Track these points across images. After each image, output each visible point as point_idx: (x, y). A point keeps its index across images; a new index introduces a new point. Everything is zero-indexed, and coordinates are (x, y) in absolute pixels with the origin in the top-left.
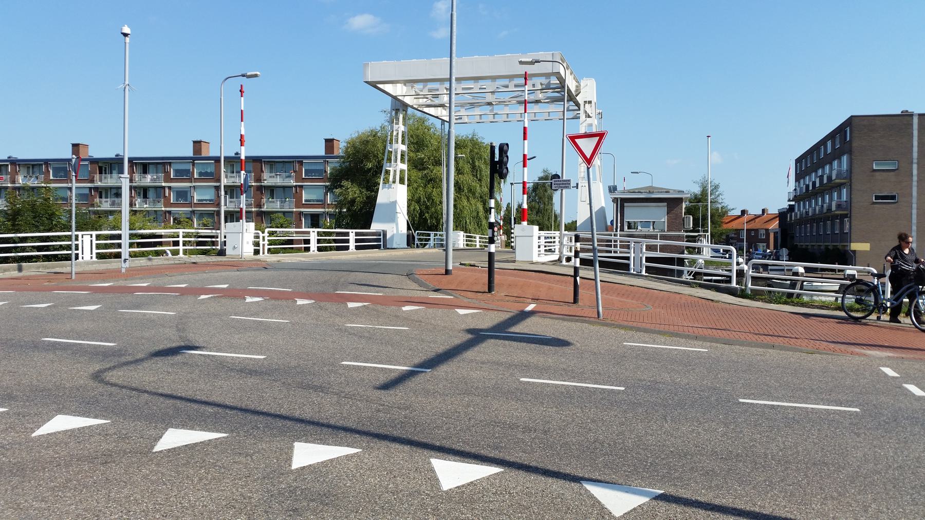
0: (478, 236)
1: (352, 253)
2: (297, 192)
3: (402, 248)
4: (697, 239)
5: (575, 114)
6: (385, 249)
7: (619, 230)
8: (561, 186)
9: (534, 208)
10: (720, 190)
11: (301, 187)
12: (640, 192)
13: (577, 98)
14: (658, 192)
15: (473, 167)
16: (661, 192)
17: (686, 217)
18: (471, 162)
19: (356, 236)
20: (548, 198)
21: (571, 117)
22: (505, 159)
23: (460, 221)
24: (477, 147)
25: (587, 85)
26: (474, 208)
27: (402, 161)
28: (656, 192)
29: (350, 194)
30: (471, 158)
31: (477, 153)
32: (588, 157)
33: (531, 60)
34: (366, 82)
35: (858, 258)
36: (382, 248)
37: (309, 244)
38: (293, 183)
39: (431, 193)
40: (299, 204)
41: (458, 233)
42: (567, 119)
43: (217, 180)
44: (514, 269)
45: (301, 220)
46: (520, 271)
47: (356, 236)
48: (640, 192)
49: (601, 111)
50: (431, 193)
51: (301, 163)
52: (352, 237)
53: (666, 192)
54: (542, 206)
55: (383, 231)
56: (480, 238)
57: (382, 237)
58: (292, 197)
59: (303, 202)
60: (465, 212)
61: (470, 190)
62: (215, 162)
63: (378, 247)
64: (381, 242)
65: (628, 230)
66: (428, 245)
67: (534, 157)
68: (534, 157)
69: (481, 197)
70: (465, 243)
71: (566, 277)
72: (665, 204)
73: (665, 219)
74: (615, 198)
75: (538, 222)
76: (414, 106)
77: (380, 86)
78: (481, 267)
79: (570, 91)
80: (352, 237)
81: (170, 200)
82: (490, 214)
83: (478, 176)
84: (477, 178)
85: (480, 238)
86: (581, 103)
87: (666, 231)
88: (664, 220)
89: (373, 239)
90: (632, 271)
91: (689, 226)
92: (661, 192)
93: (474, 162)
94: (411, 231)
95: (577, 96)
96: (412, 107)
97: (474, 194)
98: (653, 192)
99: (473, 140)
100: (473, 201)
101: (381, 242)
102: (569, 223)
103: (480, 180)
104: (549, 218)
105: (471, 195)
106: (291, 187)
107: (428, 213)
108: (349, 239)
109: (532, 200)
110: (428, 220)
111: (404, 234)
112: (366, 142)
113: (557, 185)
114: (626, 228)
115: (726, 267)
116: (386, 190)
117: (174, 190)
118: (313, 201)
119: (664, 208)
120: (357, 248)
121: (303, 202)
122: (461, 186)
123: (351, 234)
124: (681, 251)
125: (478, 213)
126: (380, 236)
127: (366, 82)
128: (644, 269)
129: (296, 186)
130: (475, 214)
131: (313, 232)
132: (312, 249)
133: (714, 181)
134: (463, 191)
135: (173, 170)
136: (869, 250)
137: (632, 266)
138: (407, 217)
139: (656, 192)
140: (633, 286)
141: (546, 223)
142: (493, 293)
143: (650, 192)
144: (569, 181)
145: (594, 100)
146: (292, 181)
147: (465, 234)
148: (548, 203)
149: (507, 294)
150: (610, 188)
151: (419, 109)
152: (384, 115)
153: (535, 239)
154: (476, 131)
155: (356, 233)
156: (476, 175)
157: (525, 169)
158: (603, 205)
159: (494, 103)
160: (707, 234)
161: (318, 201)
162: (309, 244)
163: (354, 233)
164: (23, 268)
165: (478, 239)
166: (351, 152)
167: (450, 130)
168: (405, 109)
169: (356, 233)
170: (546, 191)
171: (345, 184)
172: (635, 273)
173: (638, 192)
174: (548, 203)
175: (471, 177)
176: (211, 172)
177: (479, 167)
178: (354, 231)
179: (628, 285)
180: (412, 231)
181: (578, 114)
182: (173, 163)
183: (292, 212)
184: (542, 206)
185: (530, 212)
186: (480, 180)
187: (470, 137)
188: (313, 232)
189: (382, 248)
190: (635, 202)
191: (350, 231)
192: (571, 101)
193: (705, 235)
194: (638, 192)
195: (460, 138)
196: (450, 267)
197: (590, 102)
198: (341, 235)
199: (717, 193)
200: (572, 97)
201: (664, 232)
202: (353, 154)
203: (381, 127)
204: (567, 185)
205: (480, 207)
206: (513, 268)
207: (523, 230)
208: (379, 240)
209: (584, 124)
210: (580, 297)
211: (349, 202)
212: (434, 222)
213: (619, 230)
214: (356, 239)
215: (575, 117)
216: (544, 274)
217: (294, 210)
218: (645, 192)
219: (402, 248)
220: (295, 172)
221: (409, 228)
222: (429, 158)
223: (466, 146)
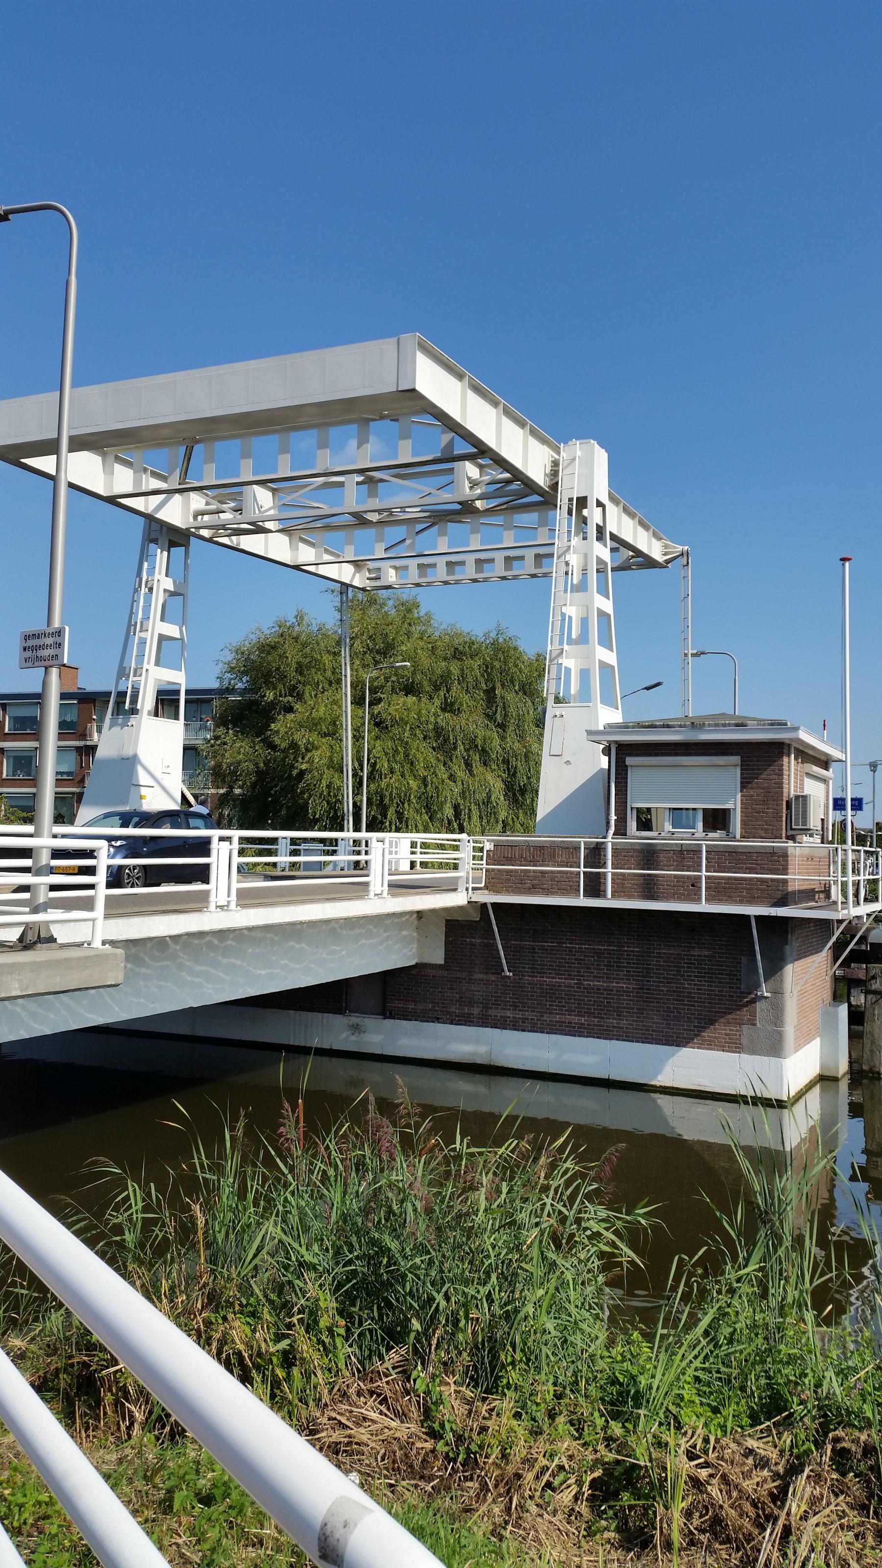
16: (724, 725)
24: (500, 655)
28: (709, 725)
35: (832, 1009)
43: (81, 735)
48: (668, 726)
53: (737, 725)
62: (79, 703)
65: (638, 834)
66: (331, 867)
72: (736, 759)
77: (123, 501)
81: (2, 773)
87: (738, 836)
92: (724, 725)
103: (502, 726)
108: (207, 867)
112: (268, 648)
114: (632, 825)
116: (117, 729)
117: (10, 754)
119: (732, 769)
123: (215, 845)
124: (779, 895)
131: (222, 839)
135: (10, 718)
136: (443, 962)
139: (709, 725)
152: (330, 596)
176: (72, 721)
177: (502, 698)
182: (10, 704)
186: (502, 726)
188: (222, 839)
190: (656, 755)
198: (162, 845)
201: (734, 839)
203: (296, 617)
218: (681, 726)
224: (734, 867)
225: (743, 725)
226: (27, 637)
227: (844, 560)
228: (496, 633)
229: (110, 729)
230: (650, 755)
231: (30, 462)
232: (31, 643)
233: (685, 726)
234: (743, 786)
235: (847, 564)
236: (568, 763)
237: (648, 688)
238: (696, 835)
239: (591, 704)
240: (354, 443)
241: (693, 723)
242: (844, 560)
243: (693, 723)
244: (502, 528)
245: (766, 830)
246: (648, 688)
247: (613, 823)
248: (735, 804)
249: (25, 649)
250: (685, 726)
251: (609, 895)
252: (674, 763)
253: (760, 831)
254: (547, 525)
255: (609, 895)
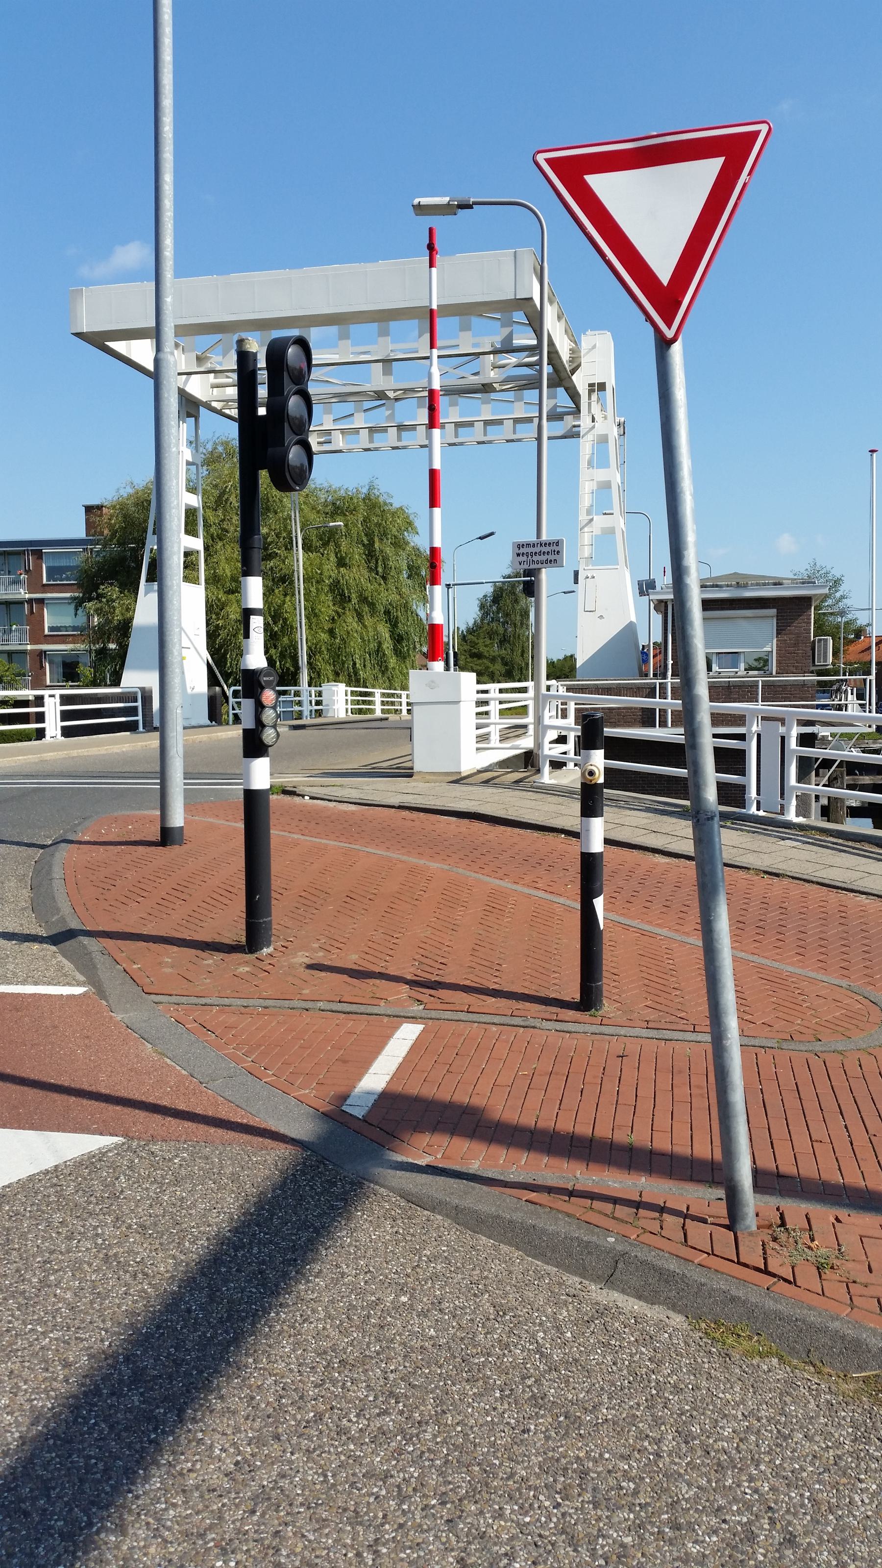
0: (378, 692)
1: (53, 747)
2: (32, 612)
3: (194, 727)
4: (835, 687)
5: (569, 427)
6: (148, 731)
7: (670, 673)
8: (535, 558)
9: (497, 633)
10: (843, 589)
11: (41, 601)
12: (717, 586)
13: (574, 378)
14: (758, 584)
15: (370, 554)
16: (764, 584)
17: (820, 640)
18: (366, 542)
19: (62, 704)
20: (521, 615)
21: (560, 433)
22: (294, 403)
23: (343, 663)
25: (594, 347)
26: (371, 634)
27: (191, 530)
28: (752, 585)
29: (117, 611)
30: (366, 535)
31: (378, 525)
32: (665, 277)
33: (445, 200)
34: (78, 335)
36: (141, 728)
37: (44, 722)
38: (23, 594)
39: (281, 606)
40: (37, 636)
41: (334, 688)
42: (549, 438)
44: (401, 807)
45: (42, 667)
46: (415, 815)
47: (62, 704)
48: (717, 586)
49: (622, 420)
50: (281, 606)
51: (39, 555)
52: (52, 708)
53: (775, 584)
54: (510, 630)
55: (143, 689)
56: (383, 695)
57: (139, 704)
58: (25, 622)
59: (46, 632)
60: (352, 644)
61: (363, 599)
63: (131, 727)
64: (137, 715)
67: (492, 534)
68: (492, 534)
69: (387, 612)
70: (350, 707)
71: (551, 836)
72: (773, 612)
73: (771, 647)
74: (660, 601)
75: (502, 659)
76: (214, 404)
77: (118, 346)
78: (312, 798)
79: (557, 352)
80: (52, 708)
82: (247, 635)
83: (380, 570)
84: (377, 574)
85: (383, 695)
86: (582, 388)
87: (774, 673)
88: (770, 649)
89: (119, 708)
90: (753, 810)
91: (825, 660)
92: (764, 584)
93: (372, 543)
94: (217, 688)
95: (573, 371)
96: (208, 406)
97: (372, 605)
98: (745, 586)
99: (370, 499)
100: (369, 621)
101: (137, 715)
102: (559, 660)
104: (523, 652)
105: (366, 609)
106: (20, 603)
107: (275, 647)
108: (63, 720)
109: (493, 618)
110: (276, 662)
111: (199, 695)
113: (525, 558)
115: (874, 743)
118: (66, 628)
120: (67, 732)
121: (46, 632)
122: (343, 591)
123: (47, 700)
125: (380, 644)
126: (136, 701)
127: (78, 335)
128: (794, 802)
129: (30, 601)
130: (373, 645)
131: (51, 696)
132: (48, 733)
133: (833, 572)
134: (350, 601)
137: (753, 793)
138: (206, 655)
139: (752, 585)
140: (777, 875)
141: (518, 660)
142: (265, 951)
143: (738, 585)
144: (557, 543)
145: (611, 383)
146: (21, 590)
147: (349, 689)
148: (522, 624)
149: (320, 957)
150: (640, 584)
151: (227, 411)
153: (468, 711)
154: (376, 482)
155: (62, 696)
156: (376, 567)
157: (437, 511)
158: (633, 619)
159: (391, 394)
160: (869, 678)
161: (74, 628)
162: (44, 722)
163: (58, 697)
164: (558, 656)
165: (378, 699)
166: (117, 526)
167: (161, 355)
168: (192, 412)
169: (62, 696)
170: (516, 601)
171: (106, 590)
172: (761, 813)
173: (713, 586)
174: (522, 624)
175: (367, 575)
178: (58, 692)
179: (758, 871)
180: (220, 685)
181: (574, 426)
183: (24, 652)
184: (510, 630)
185: (488, 642)
186: (384, 578)
187: (365, 490)
188: (51, 696)
189: (141, 728)
191: (46, 693)
192: (559, 385)
193: (865, 680)
194: (713, 586)
195: (342, 493)
196: (177, 819)
197: (602, 387)
199: (838, 595)
200: (563, 375)
201: (771, 675)
202: (121, 528)
204: (551, 557)
205: (384, 631)
206: (395, 800)
207: (432, 685)
208: (133, 711)
209: (590, 437)
210: (607, 983)
211: (117, 628)
212: (288, 665)
213: (670, 673)
214: (63, 712)
215: (570, 434)
216: (484, 826)
217: (29, 647)
218: (728, 586)
219: (194, 727)
220: (27, 572)
221: (213, 681)
222: (278, 535)
223: (355, 510)
224: (772, 698)
225: (780, 584)
226: (520, 546)
227: (872, 451)
228: (367, 487)
229: (146, 594)
230: (734, 609)
231: (112, 345)
232: (522, 550)
233: (731, 586)
234: (778, 634)
235: (875, 455)
236: (601, 617)
237: (481, 538)
238: (739, 674)
239: (618, 567)
240: (416, 333)
241: (738, 583)
242: (872, 451)
243: (738, 583)
244: (480, 401)
245: (797, 667)
246: (481, 538)
247: (670, 667)
248: (772, 648)
249: (518, 555)
250: (731, 586)
251: (670, 725)
252: (712, 616)
253: (791, 668)
254: (522, 400)
255: (670, 725)
